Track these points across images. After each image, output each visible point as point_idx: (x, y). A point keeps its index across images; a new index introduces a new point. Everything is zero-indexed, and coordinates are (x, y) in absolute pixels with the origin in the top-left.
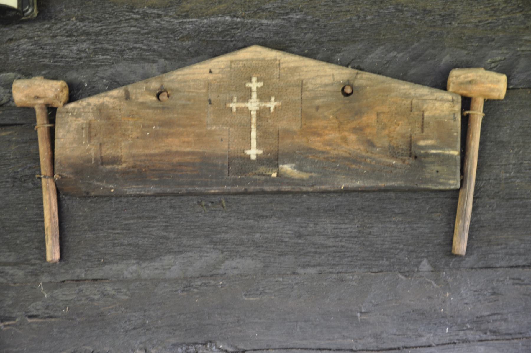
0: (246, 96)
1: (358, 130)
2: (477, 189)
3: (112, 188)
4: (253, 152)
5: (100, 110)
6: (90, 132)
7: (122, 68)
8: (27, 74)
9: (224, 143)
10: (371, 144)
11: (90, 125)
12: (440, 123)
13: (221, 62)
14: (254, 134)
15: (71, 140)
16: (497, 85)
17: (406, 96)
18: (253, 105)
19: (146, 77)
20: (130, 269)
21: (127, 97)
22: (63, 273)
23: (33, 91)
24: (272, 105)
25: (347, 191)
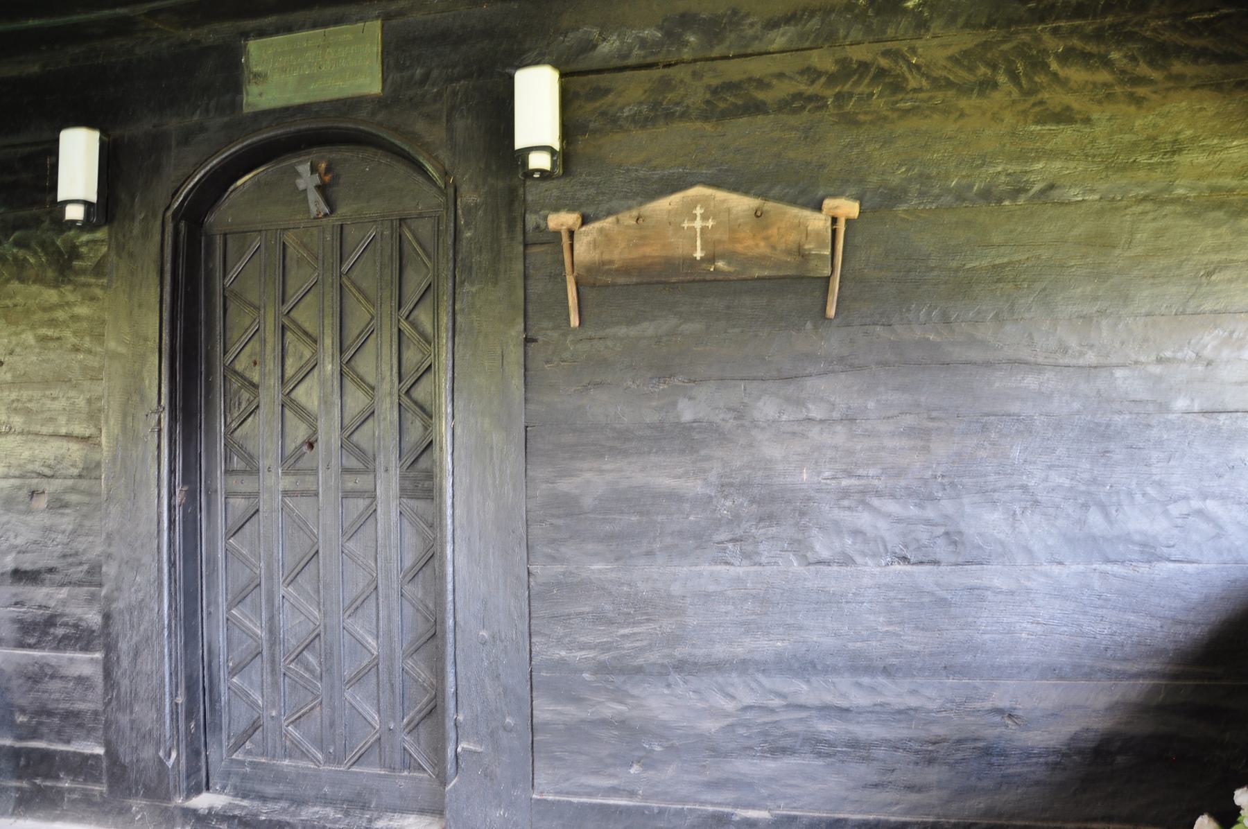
0: (694, 218)
1: (766, 238)
2: (841, 276)
3: (609, 280)
4: (699, 254)
5: (601, 230)
6: (595, 244)
7: (615, 204)
8: (556, 209)
10: (774, 248)
11: (595, 241)
12: (818, 233)
13: (676, 198)
14: (699, 243)
15: (584, 249)
17: (796, 216)
19: (629, 208)
20: (622, 331)
21: (618, 221)
23: (562, 220)
24: (710, 223)
25: (759, 279)
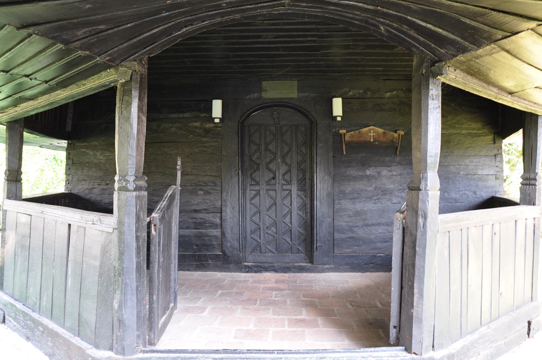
6: (350, 137)
9: (368, 139)
13: (367, 128)
15: (347, 138)
16: (403, 133)
18: (372, 134)
22: (255, 185)
